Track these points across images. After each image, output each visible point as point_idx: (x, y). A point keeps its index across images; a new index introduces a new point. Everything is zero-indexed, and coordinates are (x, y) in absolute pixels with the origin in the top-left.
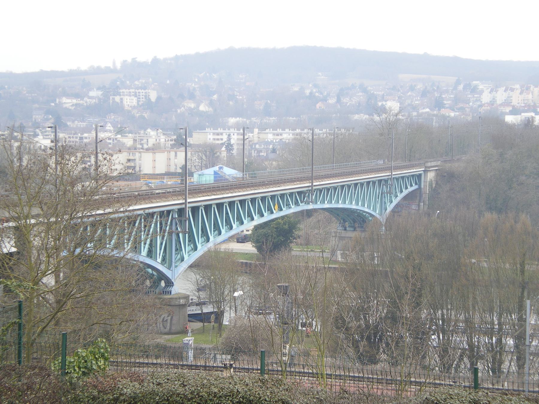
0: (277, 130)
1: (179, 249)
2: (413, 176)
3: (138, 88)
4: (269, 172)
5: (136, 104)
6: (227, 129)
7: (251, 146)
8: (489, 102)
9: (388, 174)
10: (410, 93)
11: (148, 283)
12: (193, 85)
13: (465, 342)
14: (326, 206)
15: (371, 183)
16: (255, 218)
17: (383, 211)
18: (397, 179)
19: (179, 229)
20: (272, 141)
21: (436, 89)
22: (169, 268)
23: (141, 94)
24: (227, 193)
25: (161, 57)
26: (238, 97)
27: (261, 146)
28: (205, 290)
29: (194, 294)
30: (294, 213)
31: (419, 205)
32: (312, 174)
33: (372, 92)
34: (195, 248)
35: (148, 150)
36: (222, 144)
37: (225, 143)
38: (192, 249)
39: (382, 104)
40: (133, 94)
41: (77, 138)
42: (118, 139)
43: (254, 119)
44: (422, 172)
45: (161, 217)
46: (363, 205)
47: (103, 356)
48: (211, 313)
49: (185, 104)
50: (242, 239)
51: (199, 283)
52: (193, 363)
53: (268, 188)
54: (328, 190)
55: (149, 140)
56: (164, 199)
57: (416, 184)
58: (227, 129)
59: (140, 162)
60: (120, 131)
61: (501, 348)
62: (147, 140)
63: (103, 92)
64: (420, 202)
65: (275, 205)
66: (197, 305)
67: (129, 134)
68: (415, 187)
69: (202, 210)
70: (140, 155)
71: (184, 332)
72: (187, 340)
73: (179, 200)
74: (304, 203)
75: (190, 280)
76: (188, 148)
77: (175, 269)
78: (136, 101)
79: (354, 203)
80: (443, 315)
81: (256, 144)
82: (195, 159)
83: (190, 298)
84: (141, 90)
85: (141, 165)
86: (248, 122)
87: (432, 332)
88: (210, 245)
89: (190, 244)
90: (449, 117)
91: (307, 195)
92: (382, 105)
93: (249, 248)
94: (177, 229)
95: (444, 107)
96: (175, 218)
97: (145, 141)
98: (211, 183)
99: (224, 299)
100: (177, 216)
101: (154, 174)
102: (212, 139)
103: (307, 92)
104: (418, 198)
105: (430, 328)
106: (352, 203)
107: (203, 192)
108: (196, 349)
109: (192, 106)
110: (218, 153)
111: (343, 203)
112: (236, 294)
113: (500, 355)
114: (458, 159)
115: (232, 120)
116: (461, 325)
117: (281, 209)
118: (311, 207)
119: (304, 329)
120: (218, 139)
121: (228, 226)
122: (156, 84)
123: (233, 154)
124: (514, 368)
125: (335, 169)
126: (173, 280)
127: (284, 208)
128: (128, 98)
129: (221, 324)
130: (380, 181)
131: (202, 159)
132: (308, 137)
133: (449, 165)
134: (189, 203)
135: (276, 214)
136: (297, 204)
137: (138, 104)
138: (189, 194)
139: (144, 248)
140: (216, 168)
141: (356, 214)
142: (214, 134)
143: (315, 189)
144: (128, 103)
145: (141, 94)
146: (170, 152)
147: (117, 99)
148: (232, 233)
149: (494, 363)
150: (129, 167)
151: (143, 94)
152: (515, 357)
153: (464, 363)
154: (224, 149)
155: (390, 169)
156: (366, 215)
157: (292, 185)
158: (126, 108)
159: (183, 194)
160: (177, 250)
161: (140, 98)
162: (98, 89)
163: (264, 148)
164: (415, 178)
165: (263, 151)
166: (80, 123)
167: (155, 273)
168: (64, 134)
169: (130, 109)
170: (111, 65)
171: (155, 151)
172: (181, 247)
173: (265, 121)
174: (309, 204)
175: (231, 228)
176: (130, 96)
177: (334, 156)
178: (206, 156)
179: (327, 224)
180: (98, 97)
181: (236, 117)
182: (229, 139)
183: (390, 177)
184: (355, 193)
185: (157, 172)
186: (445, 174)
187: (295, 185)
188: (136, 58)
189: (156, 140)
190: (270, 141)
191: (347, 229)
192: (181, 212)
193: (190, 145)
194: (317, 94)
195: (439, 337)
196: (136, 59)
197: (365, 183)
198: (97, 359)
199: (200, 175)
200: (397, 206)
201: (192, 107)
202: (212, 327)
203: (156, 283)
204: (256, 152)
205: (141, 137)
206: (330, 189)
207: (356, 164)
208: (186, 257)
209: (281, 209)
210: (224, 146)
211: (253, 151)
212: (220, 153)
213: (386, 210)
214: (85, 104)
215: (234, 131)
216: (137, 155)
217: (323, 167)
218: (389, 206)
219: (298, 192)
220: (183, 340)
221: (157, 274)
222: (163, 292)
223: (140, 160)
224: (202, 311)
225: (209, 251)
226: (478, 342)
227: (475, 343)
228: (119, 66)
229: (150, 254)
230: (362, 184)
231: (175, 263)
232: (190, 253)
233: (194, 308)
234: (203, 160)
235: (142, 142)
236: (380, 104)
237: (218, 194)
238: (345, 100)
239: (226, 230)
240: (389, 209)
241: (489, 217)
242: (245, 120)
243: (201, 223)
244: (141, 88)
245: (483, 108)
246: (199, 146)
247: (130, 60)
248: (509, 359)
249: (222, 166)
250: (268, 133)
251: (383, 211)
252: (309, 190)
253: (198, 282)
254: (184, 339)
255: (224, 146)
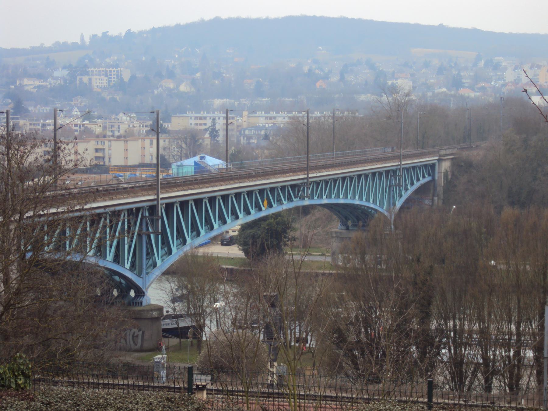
0: (270, 113)
1: (150, 254)
2: (425, 166)
3: (109, 66)
4: (260, 162)
5: (107, 85)
6: (211, 112)
7: (240, 132)
8: (513, 81)
9: (397, 164)
10: (424, 70)
11: (115, 293)
12: (173, 62)
13: (479, 356)
14: (325, 201)
15: (377, 174)
16: (241, 216)
17: (392, 207)
18: (408, 170)
19: (150, 230)
20: (264, 126)
21: (453, 65)
22: (139, 275)
23: (113, 73)
24: (207, 187)
25: (135, 29)
26: (224, 75)
27: (251, 132)
28: (182, 301)
29: (169, 307)
30: (286, 210)
31: (433, 200)
32: (308, 163)
33: (381, 69)
34: (170, 252)
35: (119, 137)
36: (206, 130)
37: (209, 128)
38: (166, 253)
39: (393, 82)
40: (104, 73)
41: (39, 125)
42: (85, 126)
43: (243, 101)
44: (436, 161)
45: (129, 215)
46: (368, 200)
47: (23, 374)
48: (188, 328)
49: (163, 84)
50: (229, 242)
51: (174, 293)
52: (166, 385)
53: (255, 181)
54: (327, 182)
55: (121, 126)
56: (132, 195)
57: (429, 175)
58: (211, 112)
59: (110, 152)
60: (87, 115)
61: (519, 361)
62: (119, 126)
63: (69, 71)
64: (434, 196)
65: (264, 200)
66: (173, 318)
67: (98, 119)
68: (428, 179)
69: (177, 207)
70: (110, 144)
71: (157, 349)
72: (159, 358)
73: (150, 195)
74: (299, 198)
75: (164, 289)
76: (160, 135)
77: (146, 277)
78: (107, 82)
79: (357, 197)
80: (455, 326)
81: (245, 130)
82: (174, 148)
83: (165, 310)
84: (113, 68)
85: (111, 156)
86: (236, 103)
87: (442, 346)
88: (187, 248)
89: (164, 247)
90: (468, 97)
91: (302, 188)
92: (392, 83)
93: (235, 251)
94: (148, 229)
95: (463, 87)
96: (146, 217)
97: (116, 127)
98: (188, 175)
99: (204, 311)
100: (147, 215)
101: (126, 166)
102: (193, 125)
103: (306, 69)
104: (432, 191)
105: (440, 341)
106: (354, 198)
107: (179, 186)
108: (169, 368)
109: (172, 86)
110: (201, 141)
111: (344, 197)
112: (218, 305)
113: (519, 369)
114: (477, 146)
115: (217, 102)
116: (475, 336)
117: (270, 206)
118: (307, 202)
119: (297, 345)
120: (201, 125)
121: (208, 226)
122: (130, 61)
123: (218, 141)
124: (533, 384)
125: (336, 157)
126: (144, 290)
127: (275, 203)
128: (98, 77)
129: (200, 341)
130: (387, 172)
131: (181, 147)
132: (303, 121)
133: (467, 153)
134: (162, 199)
135: (265, 212)
136: (290, 199)
137: (109, 85)
138: (162, 188)
139: (110, 251)
140: (197, 159)
141: (360, 211)
142: (196, 118)
143: (311, 182)
144: (98, 84)
145: (113, 73)
146: (144, 140)
147: (85, 79)
148: (213, 234)
149: (511, 378)
150: (96, 158)
151: (114, 73)
152: (535, 372)
153: (478, 380)
154: (207, 135)
155: (398, 158)
156: (371, 212)
157: (284, 177)
158: (95, 89)
159: (155, 189)
160: (148, 254)
161: (111, 78)
162: (64, 68)
163: (254, 134)
164: (428, 168)
165: (254, 138)
166: (43, 108)
167: (123, 281)
168: (25, 121)
169: (100, 90)
170: (78, 40)
171: (127, 139)
172: (153, 251)
173: (256, 102)
174: (304, 199)
175: (212, 228)
176: (100, 75)
177: (334, 143)
178: (186, 144)
179: (327, 222)
180: (64, 77)
181: (222, 98)
182: (214, 124)
183: (399, 167)
184: (358, 186)
185: (130, 162)
186: (463, 164)
187: (287, 176)
188: (108, 32)
189: (129, 126)
190: (261, 125)
191: (350, 228)
192: (153, 209)
193: (165, 131)
194: (317, 71)
195: (450, 350)
196: (107, 34)
197: (371, 175)
198: (16, 377)
199: (179, 166)
200: (408, 200)
201: (172, 88)
202: (189, 344)
203: (124, 293)
204: (245, 139)
205: (112, 122)
206: (329, 181)
207: (360, 152)
208: (159, 262)
209: (270, 206)
210: (208, 132)
211: (242, 138)
212: (203, 140)
213: (394, 205)
214: (49, 86)
215: (219, 115)
216: (107, 143)
217: (322, 156)
218: (398, 201)
219: (292, 186)
220: (154, 359)
221: (126, 282)
222: (133, 303)
223: (110, 149)
224: (178, 325)
225: (186, 256)
226: (494, 355)
227: (490, 357)
228: (87, 40)
229: (117, 259)
230: (366, 176)
231: (147, 269)
232: (164, 257)
233: (169, 321)
234: (183, 149)
235: (113, 129)
236: (390, 82)
237: (196, 189)
238: (350, 78)
239: (205, 230)
240: (399, 205)
241: (508, 212)
242: (233, 101)
243: (176, 223)
244: (112, 66)
245: (507, 87)
246: (177, 132)
247: (100, 35)
248: (529, 373)
249: (203, 155)
250: (259, 116)
251: (392, 207)
252: (305, 183)
253: (172, 292)
254: (155, 357)
255: (208, 132)
